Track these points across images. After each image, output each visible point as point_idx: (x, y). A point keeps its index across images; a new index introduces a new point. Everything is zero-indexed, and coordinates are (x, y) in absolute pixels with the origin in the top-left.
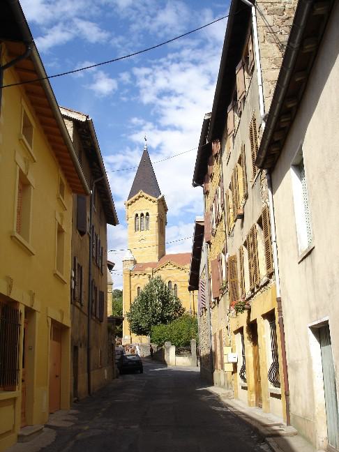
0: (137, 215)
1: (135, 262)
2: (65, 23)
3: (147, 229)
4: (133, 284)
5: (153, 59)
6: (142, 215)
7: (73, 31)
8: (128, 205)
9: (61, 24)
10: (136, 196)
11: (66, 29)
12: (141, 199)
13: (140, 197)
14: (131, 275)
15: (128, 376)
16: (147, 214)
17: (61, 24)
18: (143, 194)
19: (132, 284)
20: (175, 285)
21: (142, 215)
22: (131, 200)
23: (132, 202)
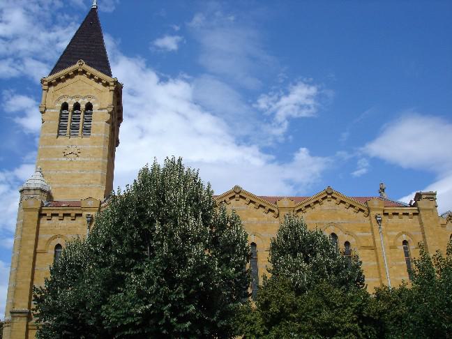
0: (65, 106)
1: (49, 196)
2: (15, 60)
3: (87, 130)
4: (44, 237)
5: (75, 63)
6: (77, 106)
7: (21, 68)
8: (50, 84)
9: (11, 60)
10: (69, 70)
11: (15, 65)
12: (78, 77)
13: (76, 72)
14: (41, 215)
15: (78, 26)
16: (89, 106)
17: (11, 60)
18: (85, 67)
19: (41, 235)
20: (347, 244)
21: (77, 106)
22: (57, 75)
23: (59, 80)
